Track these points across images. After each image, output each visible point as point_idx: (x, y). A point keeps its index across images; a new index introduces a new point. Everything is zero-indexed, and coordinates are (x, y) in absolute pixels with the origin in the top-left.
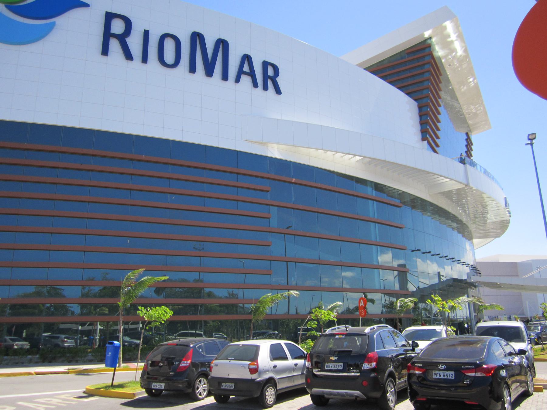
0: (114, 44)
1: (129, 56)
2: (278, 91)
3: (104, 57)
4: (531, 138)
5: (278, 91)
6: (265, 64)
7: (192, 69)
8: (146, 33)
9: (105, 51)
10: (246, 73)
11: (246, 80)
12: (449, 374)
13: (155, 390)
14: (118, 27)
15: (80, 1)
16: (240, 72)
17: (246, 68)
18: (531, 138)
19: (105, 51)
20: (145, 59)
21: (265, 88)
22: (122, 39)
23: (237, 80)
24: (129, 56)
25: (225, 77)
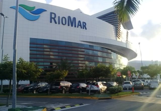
0: (53, 20)
1: (56, 23)
2: (86, 29)
3: (51, 23)
4: (139, 43)
5: (86, 29)
6: (83, 23)
7: (69, 25)
8: (59, 17)
9: (51, 22)
10: (79, 25)
11: (79, 27)
12: (99, 99)
13: (82, 87)
14: (53, 16)
15: (28, 1)
16: (78, 25)
17: (79, 24)
18: (139, 43)
19: (51, 22)
20: (59, 24)
21: (83, 28)
22: (54, 19)
23: (78, 27)
24: (56, 23)
25: (75, 27)
